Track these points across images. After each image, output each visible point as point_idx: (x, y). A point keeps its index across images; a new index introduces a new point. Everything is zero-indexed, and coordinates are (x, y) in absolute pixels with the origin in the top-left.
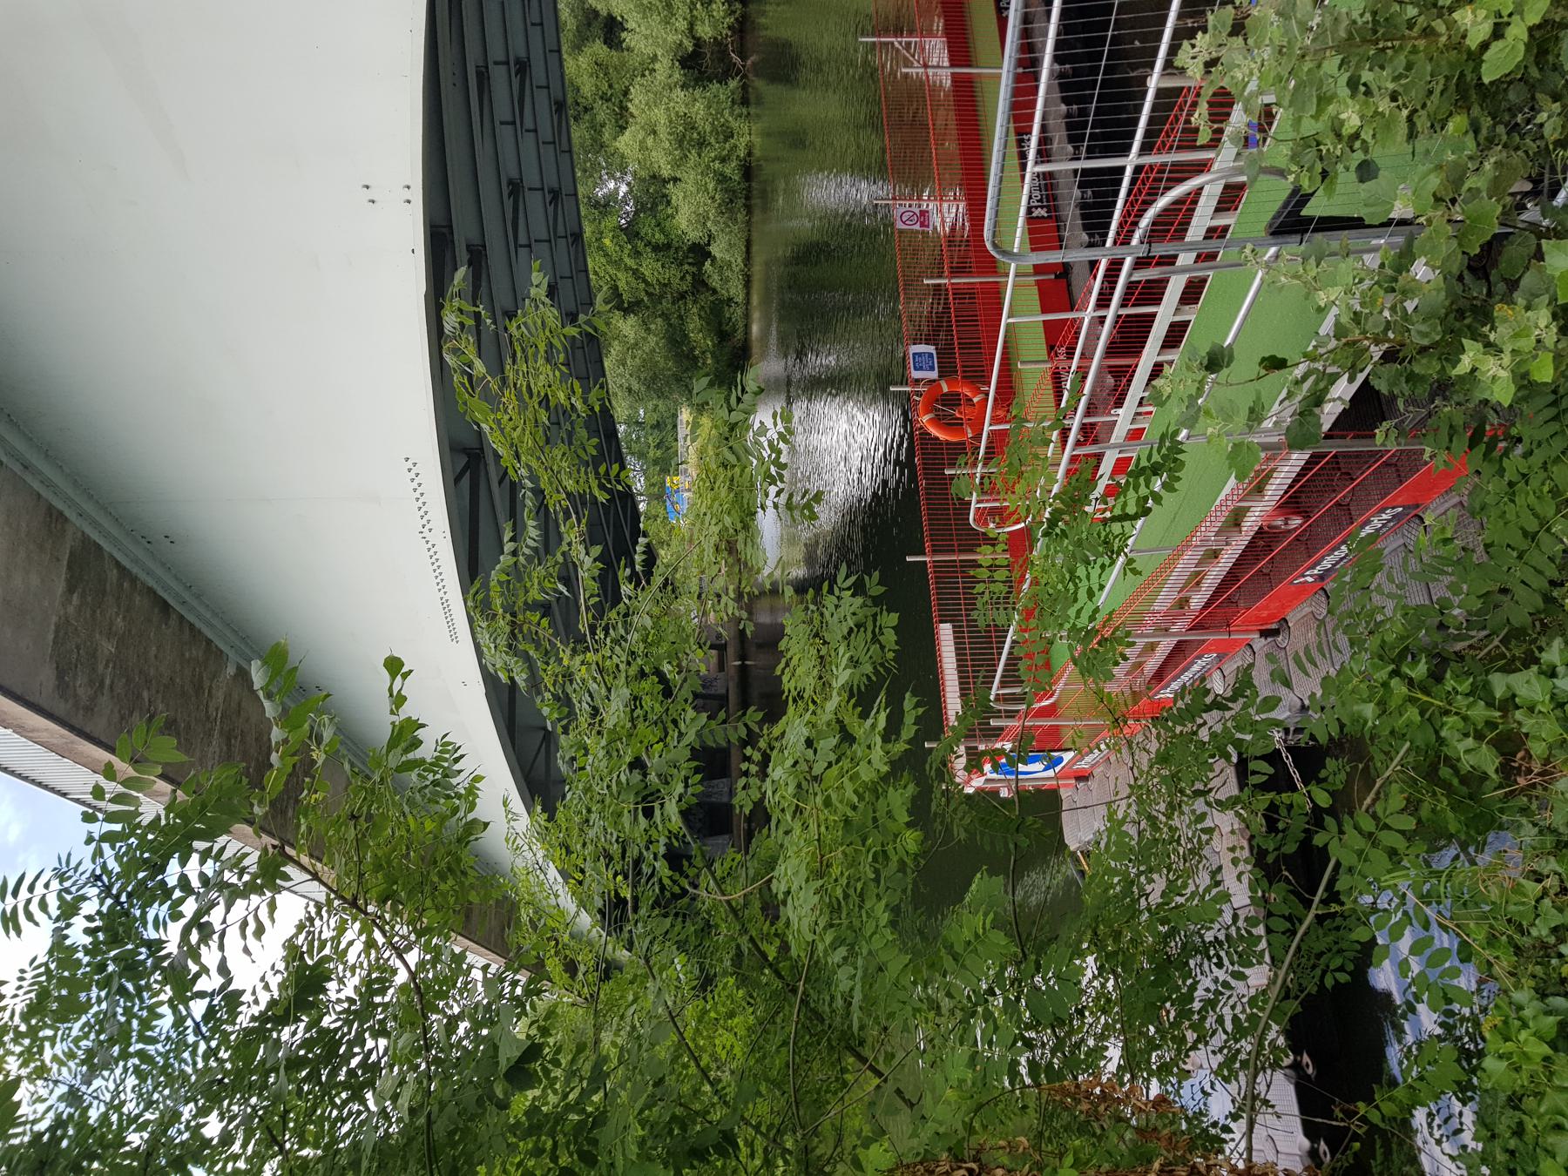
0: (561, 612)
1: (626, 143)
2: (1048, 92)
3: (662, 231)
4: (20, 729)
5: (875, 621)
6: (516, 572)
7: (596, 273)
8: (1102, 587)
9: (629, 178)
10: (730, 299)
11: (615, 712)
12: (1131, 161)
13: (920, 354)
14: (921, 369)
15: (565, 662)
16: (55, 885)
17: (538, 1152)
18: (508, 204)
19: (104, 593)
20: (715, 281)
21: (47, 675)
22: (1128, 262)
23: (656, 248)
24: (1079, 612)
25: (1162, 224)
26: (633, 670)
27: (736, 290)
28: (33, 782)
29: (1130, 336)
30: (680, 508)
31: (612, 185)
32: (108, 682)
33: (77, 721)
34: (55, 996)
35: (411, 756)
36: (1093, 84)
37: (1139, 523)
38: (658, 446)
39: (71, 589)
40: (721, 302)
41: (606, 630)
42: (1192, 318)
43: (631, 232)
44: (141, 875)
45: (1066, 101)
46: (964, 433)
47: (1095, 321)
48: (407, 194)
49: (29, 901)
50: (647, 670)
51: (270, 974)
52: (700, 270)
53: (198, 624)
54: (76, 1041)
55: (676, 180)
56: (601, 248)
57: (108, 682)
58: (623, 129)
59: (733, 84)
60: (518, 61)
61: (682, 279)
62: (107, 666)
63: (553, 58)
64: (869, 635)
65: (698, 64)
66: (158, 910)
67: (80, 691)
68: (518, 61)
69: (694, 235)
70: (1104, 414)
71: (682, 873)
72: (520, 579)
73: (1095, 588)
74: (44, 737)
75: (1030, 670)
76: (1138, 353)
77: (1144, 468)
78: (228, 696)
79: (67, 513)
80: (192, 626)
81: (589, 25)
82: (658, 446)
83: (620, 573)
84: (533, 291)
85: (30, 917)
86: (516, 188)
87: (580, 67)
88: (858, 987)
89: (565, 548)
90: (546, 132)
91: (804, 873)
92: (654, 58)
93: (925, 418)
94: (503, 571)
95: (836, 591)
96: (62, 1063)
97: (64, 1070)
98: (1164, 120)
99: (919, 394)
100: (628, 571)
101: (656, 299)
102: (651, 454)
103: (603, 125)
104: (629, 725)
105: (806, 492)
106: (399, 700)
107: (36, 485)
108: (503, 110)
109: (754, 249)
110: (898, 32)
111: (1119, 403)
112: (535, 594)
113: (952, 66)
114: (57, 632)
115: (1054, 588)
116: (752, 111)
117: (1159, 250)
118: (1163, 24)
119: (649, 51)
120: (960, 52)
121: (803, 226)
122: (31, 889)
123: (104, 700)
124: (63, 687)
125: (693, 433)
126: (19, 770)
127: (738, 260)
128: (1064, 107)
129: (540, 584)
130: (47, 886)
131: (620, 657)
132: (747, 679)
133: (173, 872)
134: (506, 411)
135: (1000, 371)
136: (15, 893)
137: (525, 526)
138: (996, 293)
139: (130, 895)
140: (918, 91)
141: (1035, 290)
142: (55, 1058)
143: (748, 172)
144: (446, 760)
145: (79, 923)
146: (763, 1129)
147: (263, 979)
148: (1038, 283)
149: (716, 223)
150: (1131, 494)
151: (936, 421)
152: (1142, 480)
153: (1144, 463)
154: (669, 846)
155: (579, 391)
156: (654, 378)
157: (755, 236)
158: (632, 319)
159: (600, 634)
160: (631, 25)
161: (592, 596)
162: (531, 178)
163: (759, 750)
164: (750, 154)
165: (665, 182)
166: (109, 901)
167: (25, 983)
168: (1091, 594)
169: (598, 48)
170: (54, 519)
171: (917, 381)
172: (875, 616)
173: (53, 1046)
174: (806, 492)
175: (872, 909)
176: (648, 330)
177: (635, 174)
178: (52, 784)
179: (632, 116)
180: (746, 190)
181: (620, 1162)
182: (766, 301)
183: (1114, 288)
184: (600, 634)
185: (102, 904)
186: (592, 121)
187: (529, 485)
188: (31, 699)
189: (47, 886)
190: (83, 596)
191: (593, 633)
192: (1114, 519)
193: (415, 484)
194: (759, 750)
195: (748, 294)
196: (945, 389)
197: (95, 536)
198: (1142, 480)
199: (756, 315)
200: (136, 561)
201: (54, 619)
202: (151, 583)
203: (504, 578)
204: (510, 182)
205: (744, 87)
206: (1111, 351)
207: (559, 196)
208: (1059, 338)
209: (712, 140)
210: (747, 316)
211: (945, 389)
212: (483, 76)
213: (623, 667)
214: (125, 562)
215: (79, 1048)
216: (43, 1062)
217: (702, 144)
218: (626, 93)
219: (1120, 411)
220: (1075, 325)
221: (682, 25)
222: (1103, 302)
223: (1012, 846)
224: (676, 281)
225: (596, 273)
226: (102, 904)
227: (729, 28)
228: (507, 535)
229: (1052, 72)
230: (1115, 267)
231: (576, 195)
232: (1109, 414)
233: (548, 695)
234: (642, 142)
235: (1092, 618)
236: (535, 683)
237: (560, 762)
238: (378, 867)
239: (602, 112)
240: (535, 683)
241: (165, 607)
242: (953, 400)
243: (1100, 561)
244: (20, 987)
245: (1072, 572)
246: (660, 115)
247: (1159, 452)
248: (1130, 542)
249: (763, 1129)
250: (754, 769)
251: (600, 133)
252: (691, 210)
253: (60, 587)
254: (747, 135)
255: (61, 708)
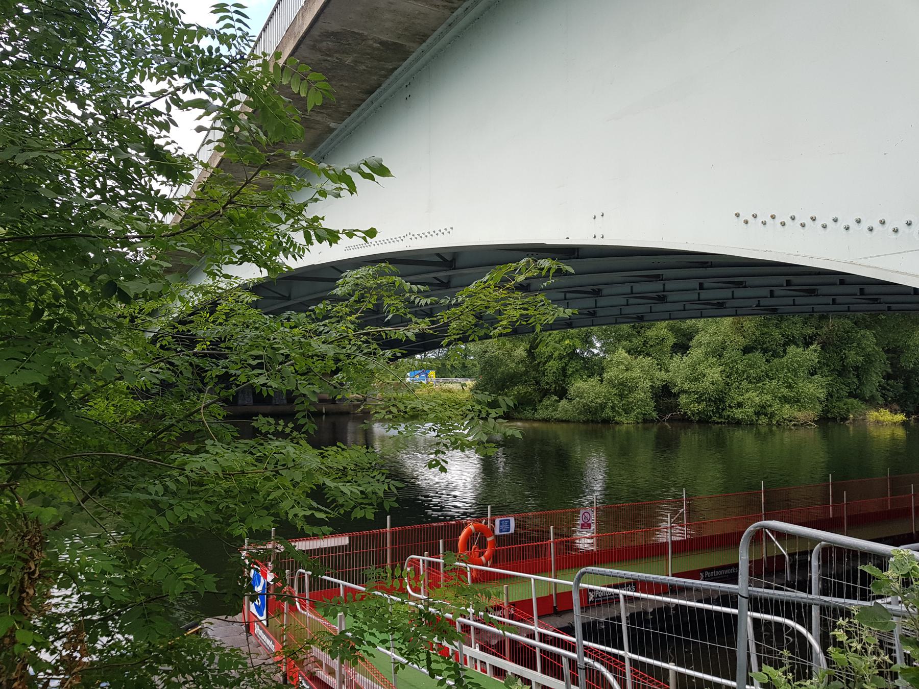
0: (375, 316)
1: (621, 354)
2: (658, 601)
3: (573, 373)
4: (304, 9)
5: (369, 504)
6: (400, 292)
7: (550, 335)
8: (388, 649)
9: (601, 355)
10: (536, 410)
11: (317, 345)
12: (626, 654)
13: (509, 524)
14: (501, 524)
15: (349, 318)
16: (239, 33)
17: (57, 297)
18: (589, 289)
19: (379, 61)
20: (546, 402)
21: (335, 27)
22: (574, 656)
23: (564, 369)
24: (373, 634)
25: (598, 678)
26: (342, 357)
27: (542, 413)
28: (272, 14)
29: (523, 655)
30: (424, 381)
31: (598, 345)
32: (329, 58)
33: (308, 41)
34: (168, 24)
35: (313, 237)
36: (662, 630)
37: (424, 670)
38: (452, 366)
39: (382, 43)
40: (535, 405)
41: (366, 342)
42: (488, 675)
43: (573, 355)
44: (241, 81)
45: (653, 613)
46: (463, 551)
47: (534, 632)
48: (599, 237)
49: (232, 19)
50: (340, 364)
51: (176, 146)
52: (553, 393)
53: (360, 109)
54: (132, 31)
55: (602, 381)
56: (564, 338)
57: (329, 58)
58: (629, 352)
59: (654, 414)
60: (665, 297)
61: (547, 383)
62: (338, 58)
63: (667, 315)
64: (360, 501)
65: (665, 394)
66: (218, 87)
67: (324, 44)
68: (665, 297)
69: (572, 390)
70: (476, 639)
71: (216, 384)
72: (396, 294)
73: (387, 645)
74: (299, 23)
75: (322, 596)
76: (512, 660)
77: (459, 674)
78: (318, 122)
79: (424, 44)
80: (359, 105)
81: (684, 335)
82: (452, 366)
83: (397, 350)
84: (561, 309)
85: (222, 19)
86: (597, 293)
87: (661, 329)
88: (148, 497)
89: (414, 319)
90: (627, 310)
91: (225, 464)
92: (667, 371)
93: (472, 527)
94: (401, 284)
95: (387, 481)
96: (119, 22)
97: (115, 23)
98: (651, 674)
99: (486, 523)
100: (399, 355)
101: (536, 368)
102: (448, 362)
103: (630, 341)
104: (310, 354)
105: (446, 462)
106: (350, 234)
107: (440, 30)
108: (639, 288)
109: (564, 425)
110: (689, 512)
111: (482, 649)
112: (387, 301)
113: (672, 542)
114: (358, 34)
115: (388, 619)
116: (640, 426)
117: (581, 675)
118: (714, 675)
119: (671, 368)
120: (680, 548)
121: (578, 451)
122: (239, 21)
123: (319, 56)
124: (327, 35)
125: (461, 387)
126: (280, 7)
127: (558, 415)
128: (651, 610)
129: (393, 305)
130: (240, 29)
131: (350, 349)
132: (333, 423)
133: (241, 97)
134: (494, 291)
135: (497, 573)
136: (237, 12)
137: (427, 297)
138: (543, 569)
139: (229, 72)
140: (651, 522)
141: (547, 594)
142: (123, 18)
143: (607, 422)
144: (294, 250)
145: (215, 43)
146: (49, 431)
147: (173, 142)
148: (551, 596)
149: (578, 403)
150: (444, 666)
151: (470, 533)
152: (453, 672)
153: (462, 674)
154: (231, 376)
155: (505, 331)
156: (491, 366)
157: (572, 426)
158: (524, 354)
159: (364, 338)
160: (685, 359)
161: (386, 334)
162: (602, 302)
163: (292, 432)
164: (616, 423)
165: (601, 375)
166: (227, 61)
167: (169, 6)
168: (384, 642)
169: (671, 340)
170: (422, 38)
171: (493, 522)
172: (371, 504)
173: (129, 17)
174: (446, 462)
175: (199, 506)
176: (518, 363)
177: (604, 358)
178: (271, 24)
179: (636, 358)
180: (596, 422)
181: (53, 351)
182: (535, 430)
183: (548, 644)
184: (364, 338)
185: (226, 57)
186: (632, 335)
187: (453, 302)
188: (322, 17)
189: (240, 29)
190: (378, 49)
191: (364, 334)
192: (428, 654)
193: (437, 232)
194: (292, 432)
195: (539, 420)
196: (489, 539)
197: (411, 58)
198: (453, 672)
199: (527, 425)
200: (397, 79)
201: (366, 33)
202: (384, 86)
203: (397, 284)
204: (600, 290)
205: (652, 421)
206: (513, 642)
207: (591, 317)
208: (521, 610)
209: (624, 402)
210: (527, 420)
211: (489, 539)
212: (658, 278)
213: (344, 350)
214: (396, 72)
215: (128, 32)
216: (121, 12)
217: (622, 396)
218: (648, 355)
219: (477, 649)
220: (530, 620)
221: (686, 386)
222: (543, 638)
223: (225, 591)
224: (546, 379)
225: (550, 335)
226: (226, 57)
227: (685, 413)
228: (422, 288)
229: (668, 604)
230: (571, 647)
231: (593, 325)
232: (476, 643)
233: (330, 307)
234: (622, 363)
235: (369, 643)
236: (336, 299)
237: (289, 312)
238: (250, 216)
239: (637, 341)
240: (336, 299)
241: (370, 92)
242: (483, 544)
243: (403, 647)
244: (167, 3)
245: (399, 630)
246: (637, 373)
247: (469, 683)
248: (415, 666)
249: (49, 431)
250: (280, 428)
251: (626, 340)
252: (585, 388)
253: (384, 38)
254: (626, 422)
255: (315, 33)
